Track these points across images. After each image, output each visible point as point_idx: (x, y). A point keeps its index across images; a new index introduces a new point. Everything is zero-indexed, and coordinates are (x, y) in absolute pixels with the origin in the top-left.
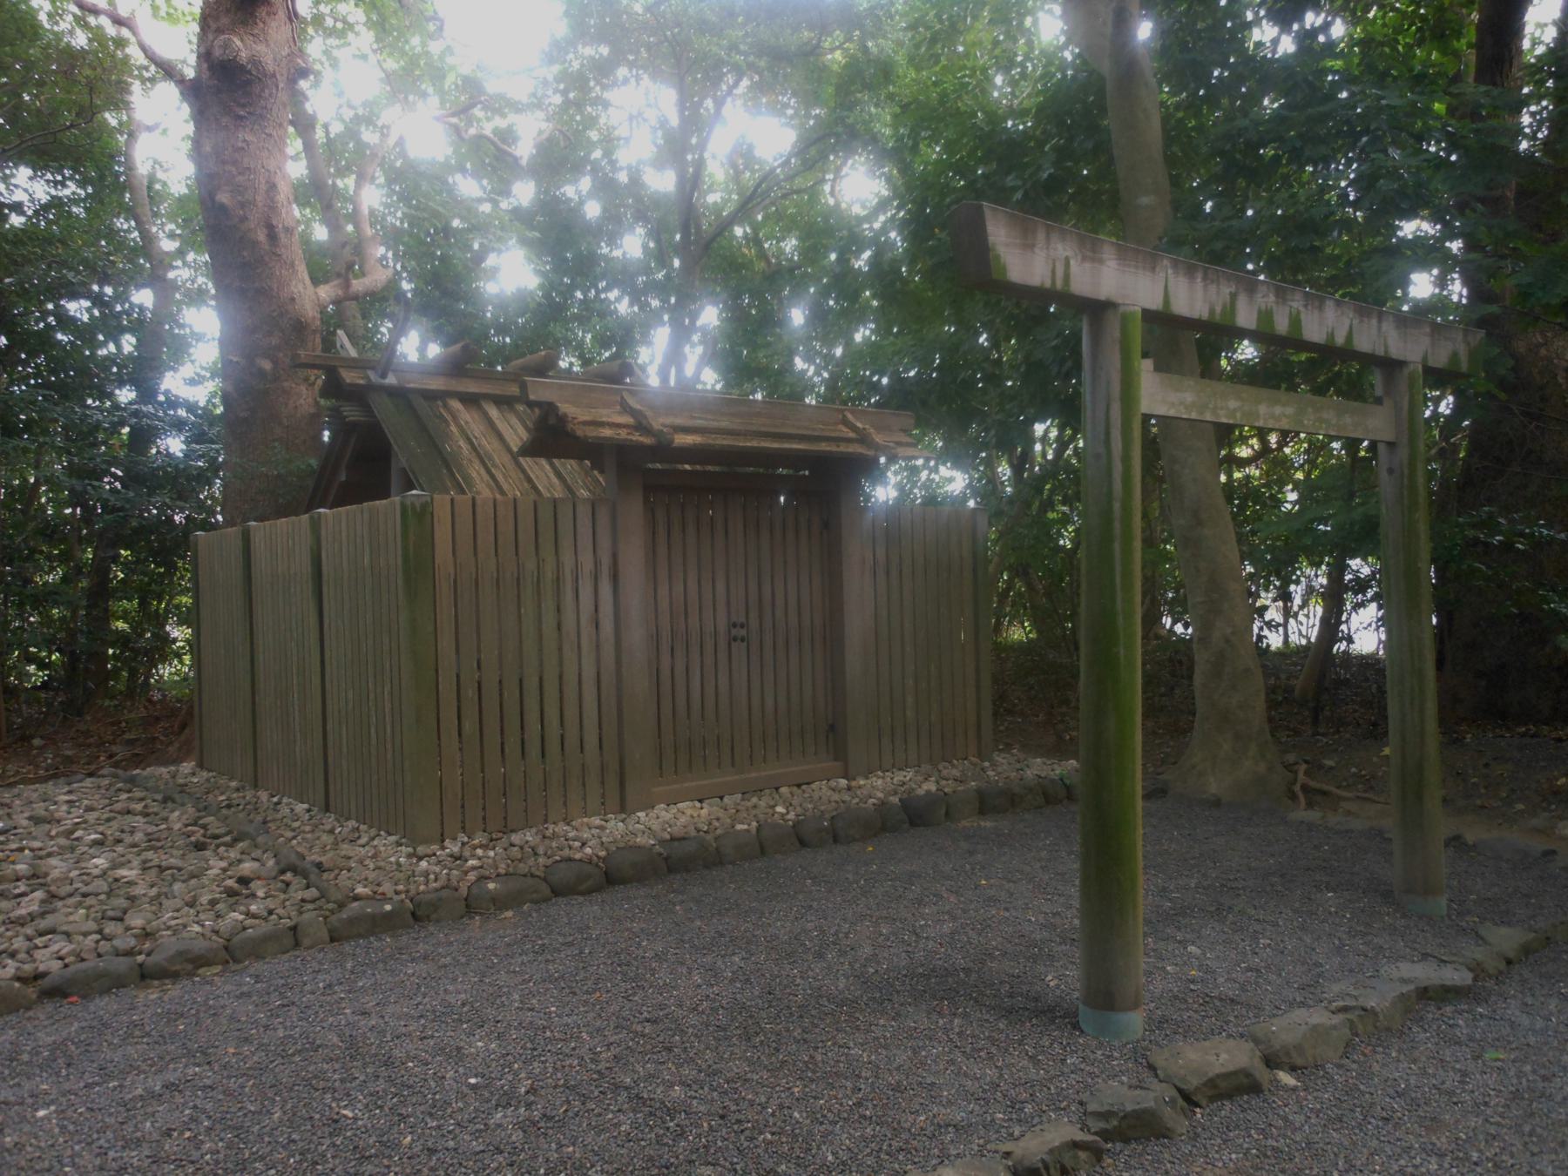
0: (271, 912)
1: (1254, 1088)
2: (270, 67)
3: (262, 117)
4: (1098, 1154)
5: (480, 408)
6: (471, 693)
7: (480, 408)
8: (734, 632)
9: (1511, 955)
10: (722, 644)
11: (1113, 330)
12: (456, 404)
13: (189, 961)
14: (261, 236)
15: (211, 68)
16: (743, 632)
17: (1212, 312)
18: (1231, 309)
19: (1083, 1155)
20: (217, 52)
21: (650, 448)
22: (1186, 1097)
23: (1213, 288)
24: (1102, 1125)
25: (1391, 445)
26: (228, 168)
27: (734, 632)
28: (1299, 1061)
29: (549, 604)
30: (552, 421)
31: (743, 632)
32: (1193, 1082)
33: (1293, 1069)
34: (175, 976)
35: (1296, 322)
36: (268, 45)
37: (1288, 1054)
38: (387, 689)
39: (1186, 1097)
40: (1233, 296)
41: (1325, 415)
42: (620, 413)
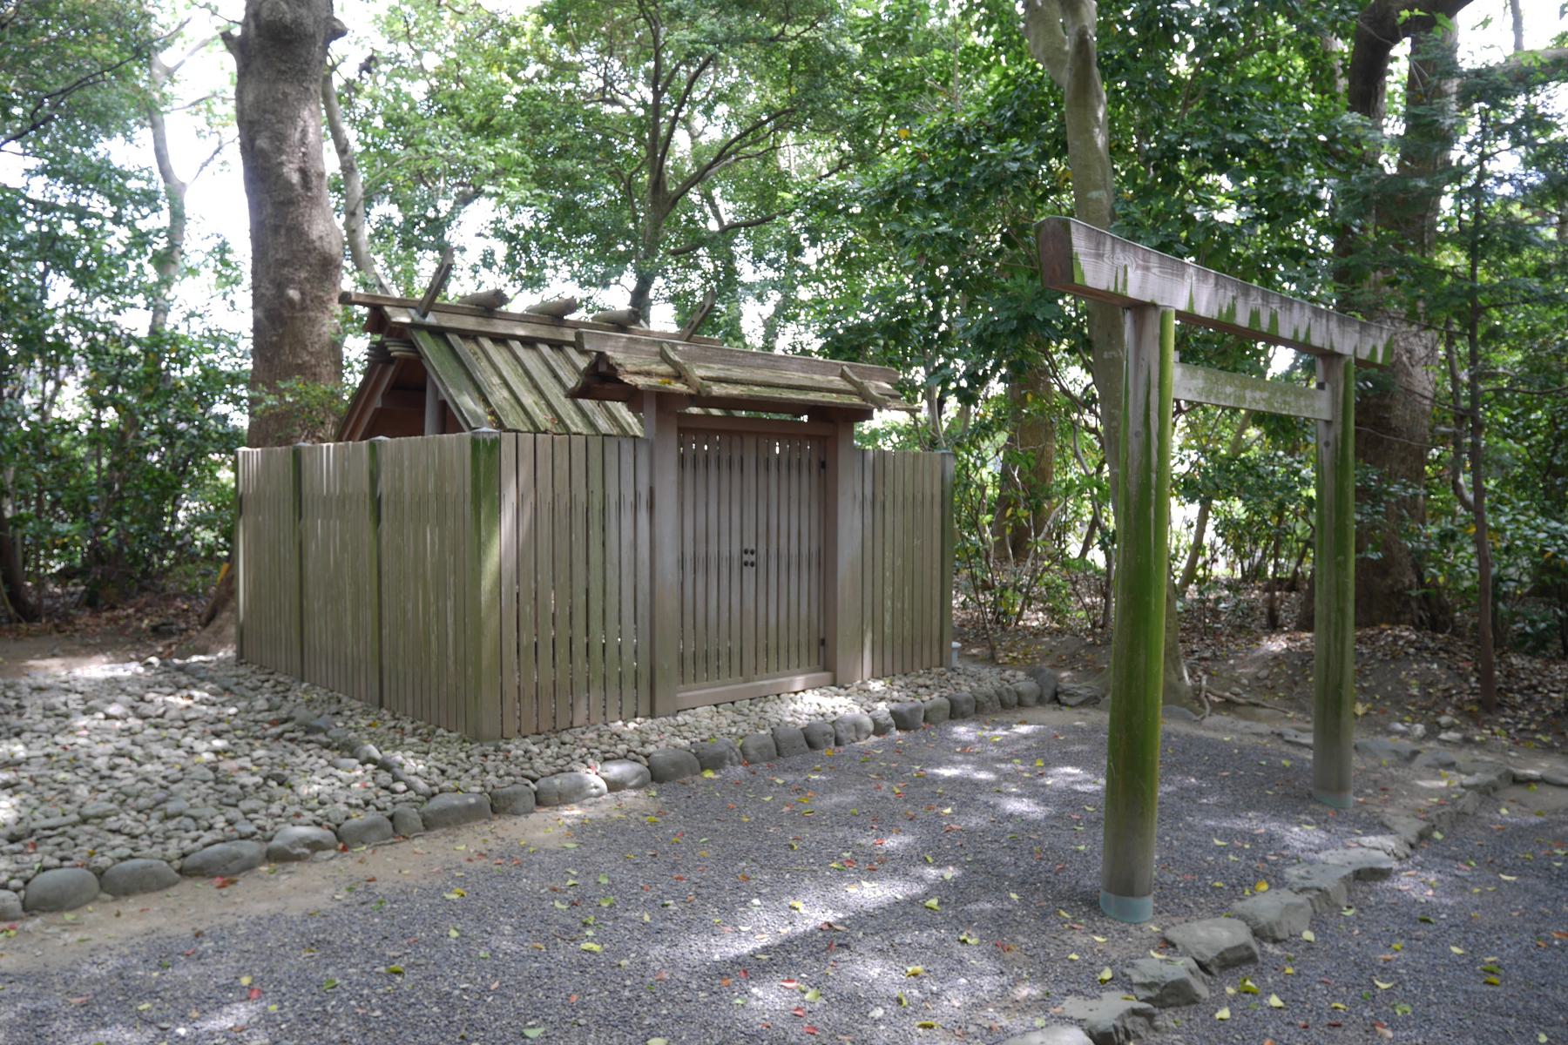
0: (367, 803)
1: (1251, 958)
2: (311, 30)
3: (304, 72)
4: (1150, 1017)
5: (477, 343)
6: (528, 609)
7: (477, 343)
8: (746, 557)
9: (1413, 840)
10: (736, 565)
11: (1152, 329)
12: (487, 344)
13: (308, 846)
14: (295, 178)
15: (257, 27)
16: (753, 558)
17: (1220, 311)
18: (1232, 311)
19: (1140, 1020)
20: (265, 14)
21: (690, 396)
22: (1203, 967)
23: (1221, 291)
24: (1148, 994)
25: (1328, 423)
26: (268, 116)
27: (746, 557)
28: (1280, 935)
29: (595, 531)
30: (603, 368)
31: (753, 558)
32: (1209, 955)
33: (1276, 941)
34: (299, 858)
35: (1274, 319)
36: (309, 9)
37: (1272, 930)
38: (450, 604)
39: (1203, 967)
40: (1234, 298)
41: (295, 178)
42: (658, 363)
